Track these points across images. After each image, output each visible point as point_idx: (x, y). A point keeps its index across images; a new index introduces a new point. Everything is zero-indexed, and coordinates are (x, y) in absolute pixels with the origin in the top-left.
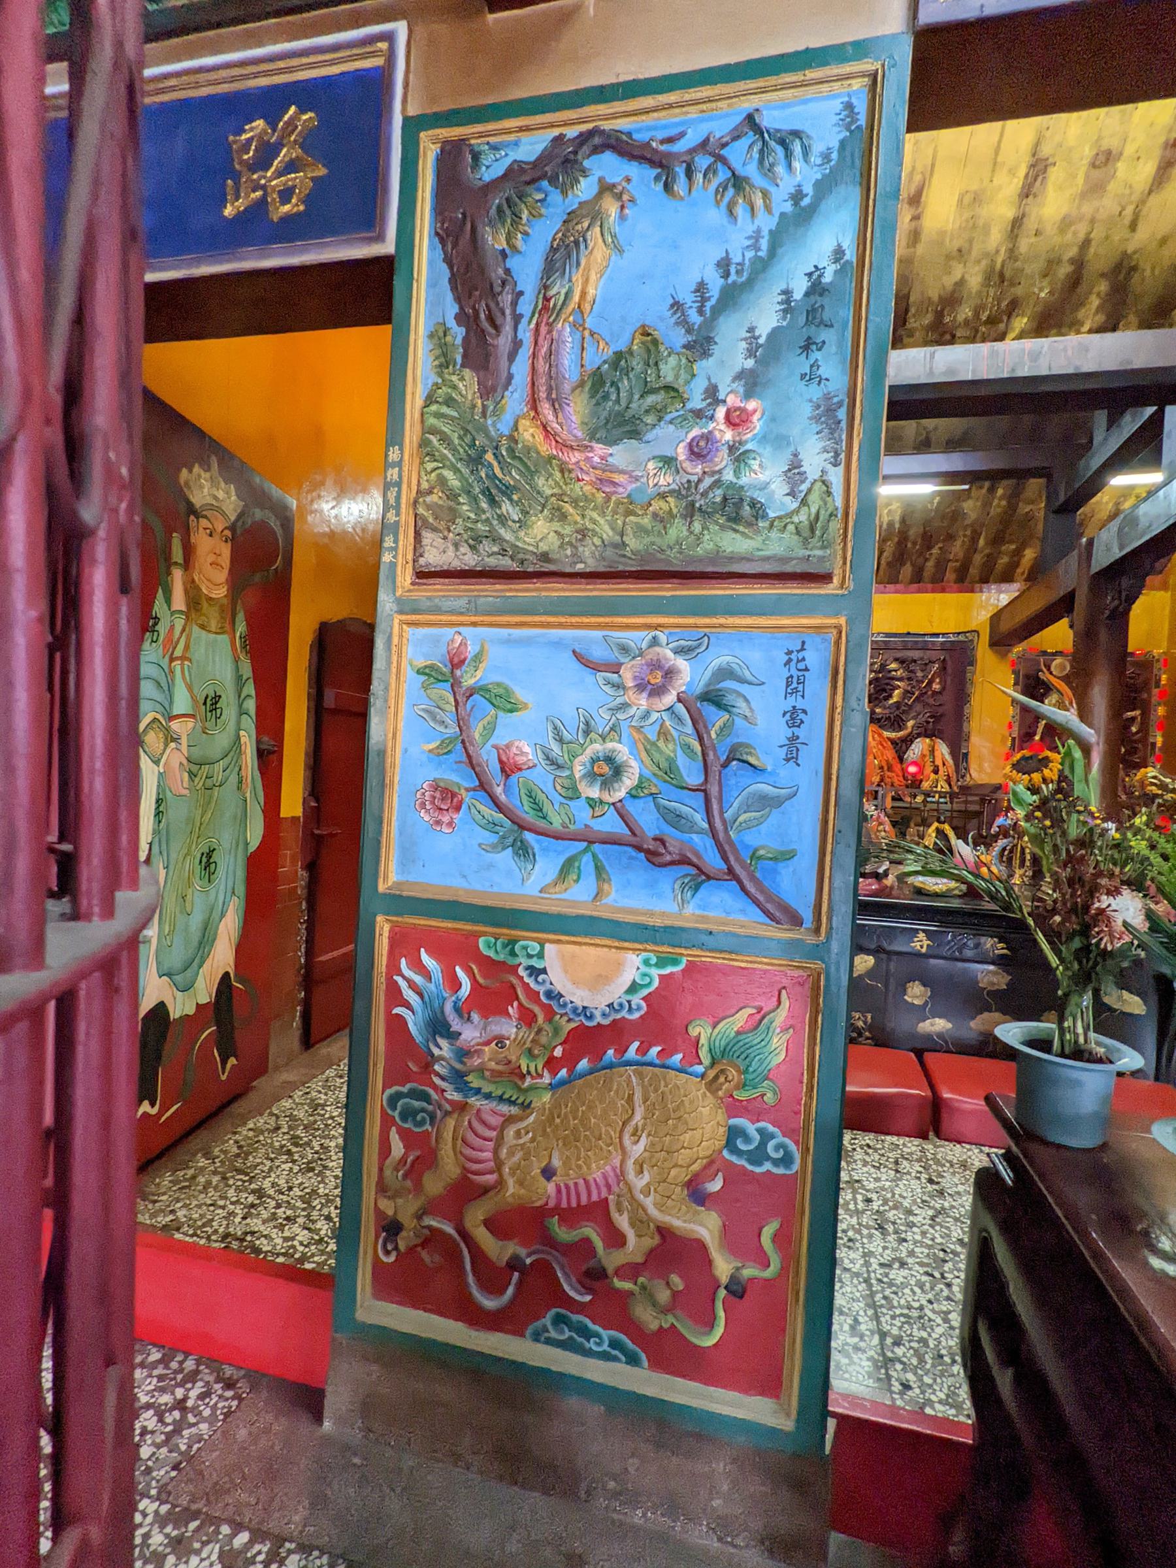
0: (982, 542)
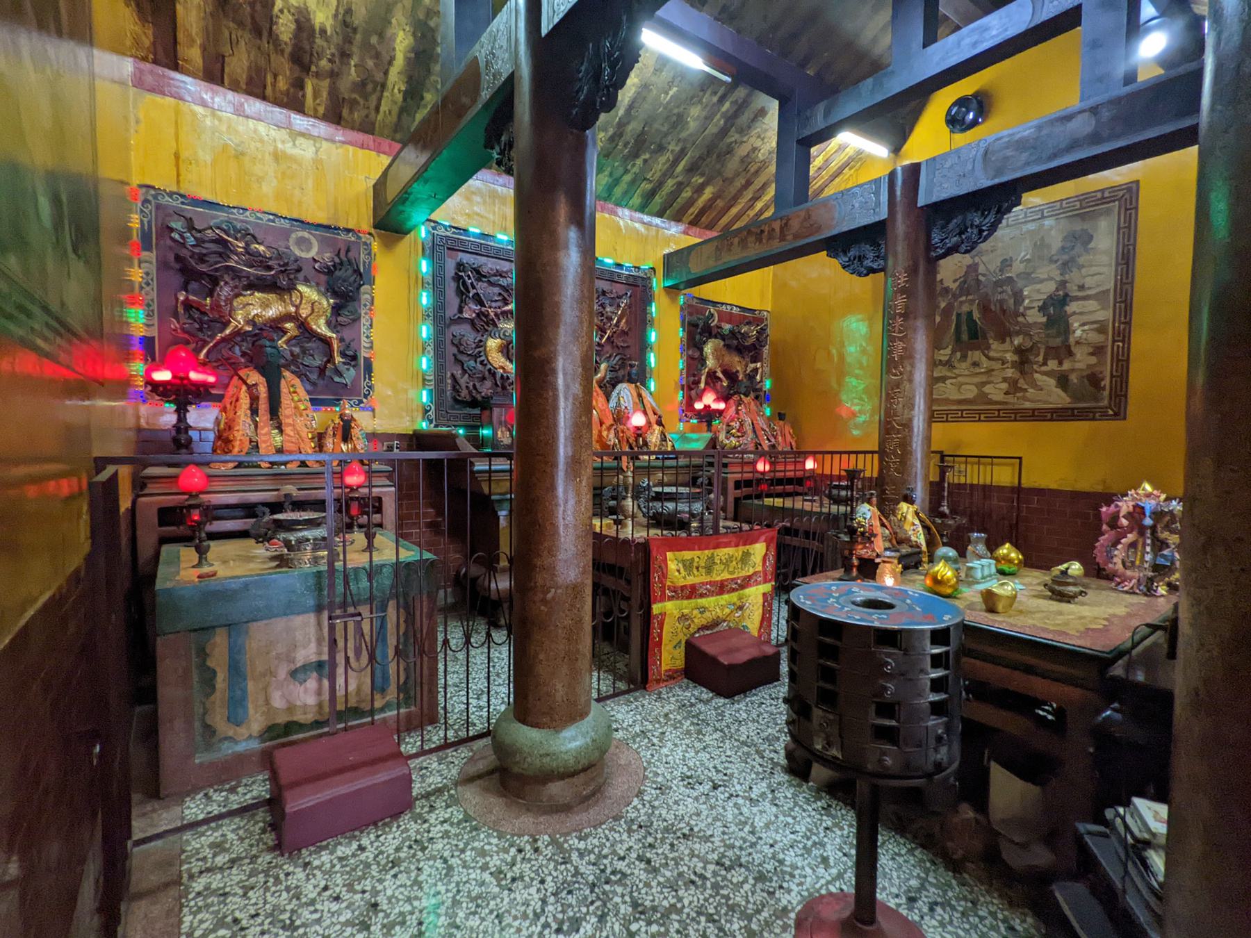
0: (680, 168)
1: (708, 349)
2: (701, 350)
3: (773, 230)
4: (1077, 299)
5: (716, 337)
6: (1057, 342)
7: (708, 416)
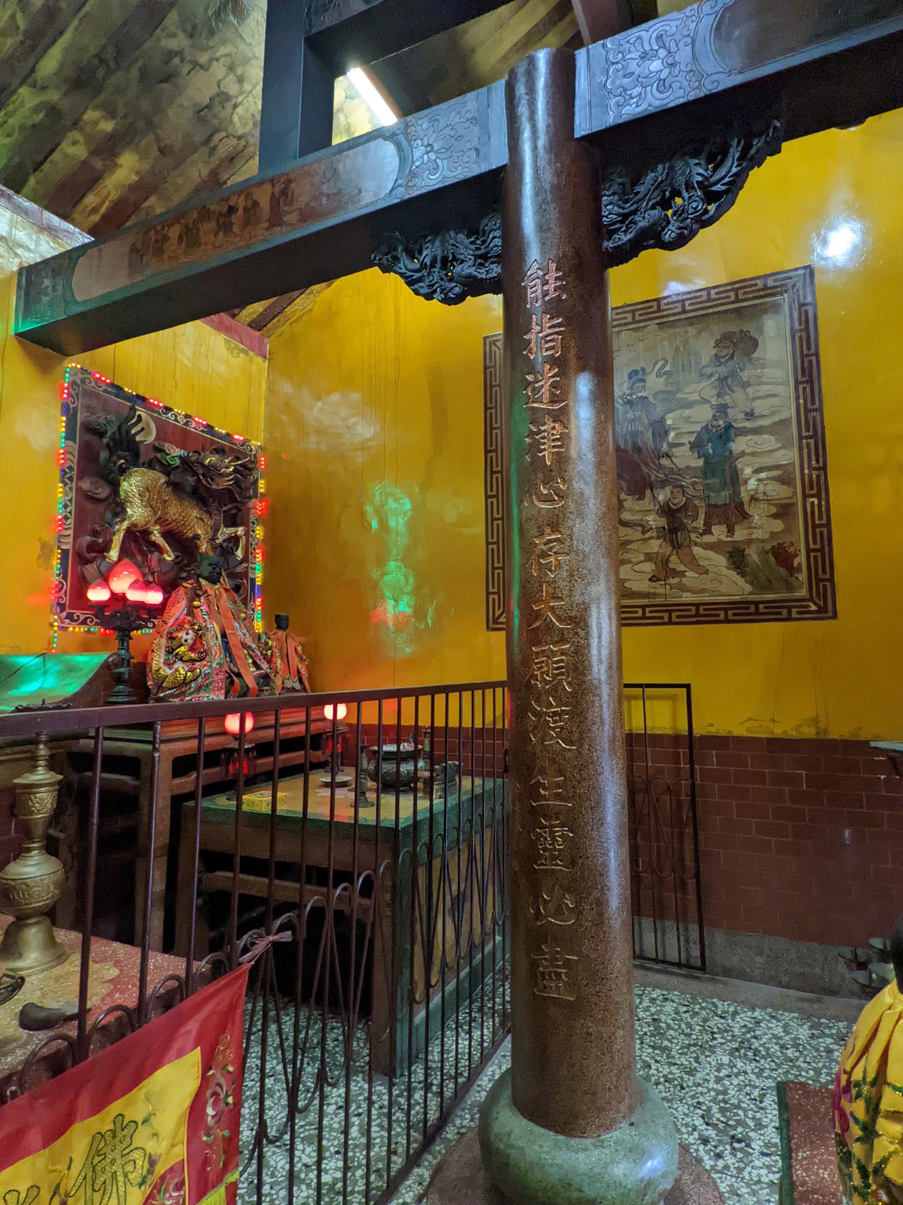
0: (51, 62)
1: (132, 484)
2: (115, 486)
3: (256, 204)
4: (744, 432)
5: (150, 465)
6: (724, 497)
7: (122, 618)
